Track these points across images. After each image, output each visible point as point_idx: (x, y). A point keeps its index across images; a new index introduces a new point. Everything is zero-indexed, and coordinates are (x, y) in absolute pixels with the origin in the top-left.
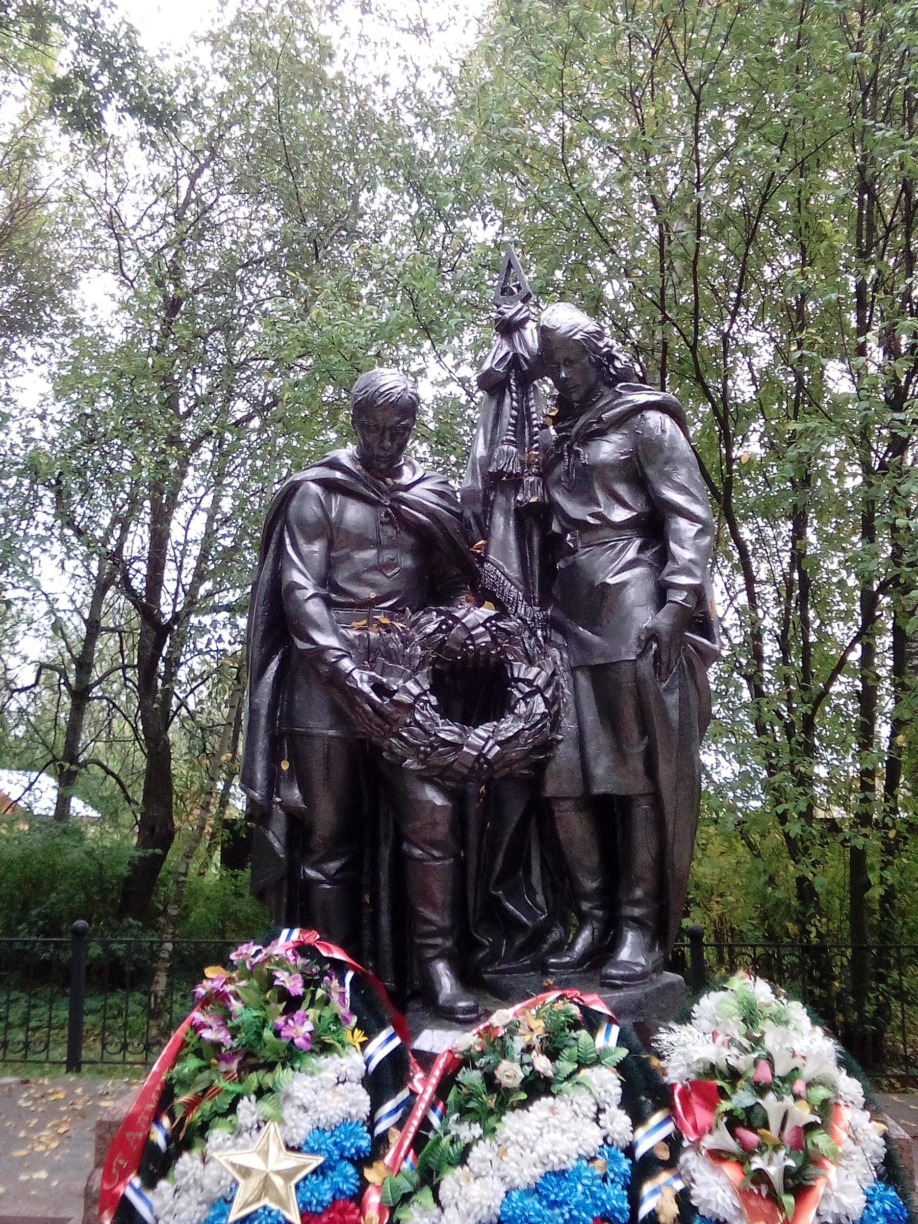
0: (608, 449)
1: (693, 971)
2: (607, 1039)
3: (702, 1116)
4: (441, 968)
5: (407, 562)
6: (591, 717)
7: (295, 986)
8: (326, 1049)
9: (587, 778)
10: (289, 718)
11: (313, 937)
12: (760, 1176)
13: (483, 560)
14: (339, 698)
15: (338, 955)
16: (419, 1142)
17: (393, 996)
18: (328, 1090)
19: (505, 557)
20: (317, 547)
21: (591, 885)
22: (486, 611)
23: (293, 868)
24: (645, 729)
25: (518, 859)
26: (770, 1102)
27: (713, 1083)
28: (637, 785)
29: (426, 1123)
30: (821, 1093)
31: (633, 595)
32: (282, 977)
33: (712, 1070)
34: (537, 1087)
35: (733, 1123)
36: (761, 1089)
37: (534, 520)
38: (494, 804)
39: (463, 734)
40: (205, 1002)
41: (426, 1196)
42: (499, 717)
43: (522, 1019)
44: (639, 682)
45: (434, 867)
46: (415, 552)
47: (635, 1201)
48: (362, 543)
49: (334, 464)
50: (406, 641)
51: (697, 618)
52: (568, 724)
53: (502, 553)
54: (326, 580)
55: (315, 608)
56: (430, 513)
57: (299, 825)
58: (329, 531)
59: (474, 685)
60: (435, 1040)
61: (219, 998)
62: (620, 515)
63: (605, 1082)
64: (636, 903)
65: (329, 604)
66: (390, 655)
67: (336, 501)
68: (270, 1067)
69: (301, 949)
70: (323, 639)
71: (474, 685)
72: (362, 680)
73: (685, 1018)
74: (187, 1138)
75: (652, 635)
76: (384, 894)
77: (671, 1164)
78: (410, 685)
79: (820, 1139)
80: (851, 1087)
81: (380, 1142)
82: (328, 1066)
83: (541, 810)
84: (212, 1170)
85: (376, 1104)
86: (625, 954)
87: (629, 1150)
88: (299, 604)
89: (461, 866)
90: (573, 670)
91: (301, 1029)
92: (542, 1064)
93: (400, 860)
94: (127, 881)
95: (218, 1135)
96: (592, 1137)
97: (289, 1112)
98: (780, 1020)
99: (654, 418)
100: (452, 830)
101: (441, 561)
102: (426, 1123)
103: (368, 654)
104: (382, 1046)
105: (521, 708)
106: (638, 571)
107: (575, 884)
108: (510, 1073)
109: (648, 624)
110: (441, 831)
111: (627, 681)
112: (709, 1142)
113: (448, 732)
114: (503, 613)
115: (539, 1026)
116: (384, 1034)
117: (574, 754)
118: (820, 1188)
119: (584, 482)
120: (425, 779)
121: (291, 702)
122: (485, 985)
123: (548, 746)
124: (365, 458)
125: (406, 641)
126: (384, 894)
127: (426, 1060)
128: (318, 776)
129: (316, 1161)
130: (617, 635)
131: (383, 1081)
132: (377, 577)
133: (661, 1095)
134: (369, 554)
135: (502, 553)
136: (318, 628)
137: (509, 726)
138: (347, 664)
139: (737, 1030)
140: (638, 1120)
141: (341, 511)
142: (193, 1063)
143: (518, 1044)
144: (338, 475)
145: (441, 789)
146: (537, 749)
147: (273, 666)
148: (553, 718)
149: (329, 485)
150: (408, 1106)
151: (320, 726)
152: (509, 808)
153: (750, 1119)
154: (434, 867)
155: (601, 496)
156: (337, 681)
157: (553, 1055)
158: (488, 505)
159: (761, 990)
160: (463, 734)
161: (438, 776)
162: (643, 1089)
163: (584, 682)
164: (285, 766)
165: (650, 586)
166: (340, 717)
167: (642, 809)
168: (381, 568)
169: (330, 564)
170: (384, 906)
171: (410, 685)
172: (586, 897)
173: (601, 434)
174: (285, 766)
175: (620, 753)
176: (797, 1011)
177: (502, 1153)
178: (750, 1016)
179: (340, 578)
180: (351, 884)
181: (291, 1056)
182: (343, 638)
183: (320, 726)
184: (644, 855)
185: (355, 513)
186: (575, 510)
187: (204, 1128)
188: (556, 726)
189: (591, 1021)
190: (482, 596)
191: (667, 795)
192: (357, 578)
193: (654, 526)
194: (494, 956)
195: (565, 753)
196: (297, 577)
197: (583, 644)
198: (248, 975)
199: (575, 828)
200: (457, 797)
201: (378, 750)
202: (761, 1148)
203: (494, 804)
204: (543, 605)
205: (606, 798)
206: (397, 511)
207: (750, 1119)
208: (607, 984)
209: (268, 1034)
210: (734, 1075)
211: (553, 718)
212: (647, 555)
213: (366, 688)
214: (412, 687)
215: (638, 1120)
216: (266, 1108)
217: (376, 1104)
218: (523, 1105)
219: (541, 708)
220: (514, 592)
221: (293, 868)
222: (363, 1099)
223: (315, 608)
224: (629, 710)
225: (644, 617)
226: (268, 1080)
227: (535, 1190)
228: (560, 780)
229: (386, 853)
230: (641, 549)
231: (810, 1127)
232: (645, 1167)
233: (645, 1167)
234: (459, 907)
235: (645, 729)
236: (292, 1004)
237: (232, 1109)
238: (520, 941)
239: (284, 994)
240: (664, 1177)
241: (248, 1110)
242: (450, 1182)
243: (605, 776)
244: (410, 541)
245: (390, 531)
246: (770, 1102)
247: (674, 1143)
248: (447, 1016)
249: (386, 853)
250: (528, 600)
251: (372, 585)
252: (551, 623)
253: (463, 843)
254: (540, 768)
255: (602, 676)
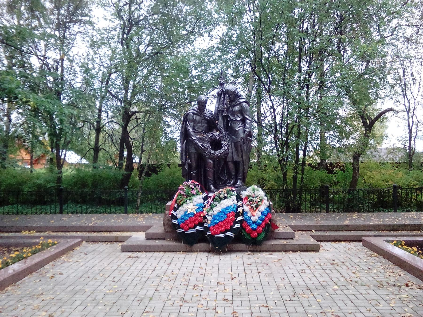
0: (237, 108)
1: (246, 185)
2: (235, 193)
3: (246, 201)
4: (211, 185)
5: (206, 125)
6: (234, 149)
7: (193, 187)
8: (197, 195)
9: (233, 159)
10: (188, 150)
11: (194, 181)
12: (252, 207)
13: (217, 124)
14: (196, 147)
15: (198, 183)
16: (210, 205)
17: (205, 188)
18: (198, 199)
19: (221, 124)
20: (192, 123)
21: (233, 174)
22: (218, 133)
23: (189, 172)
24: (242, 152)
25: (223, 170)
26: (254, 199)
27: (247, 197)
28: (240, 159)
29: (211, 203)
30: (261, 198)
31: (240, 131)
32: (191, 186)
33: (248, 196)
34: (225, 198)
35: (249, 201)
36: (253, 197)
37: (225, 118)
38: (219, 162)
39: (215, 152)
40: (180, 189)
41: (212, 210)
42: (220, 150)
43: (223, 191)
44: (241, 145)
45: (210, 172)
46: (207, 123)
47: (237, 210)
48: (199, 123)
49: (194, 110)
50: (206, 138)
51: (250, 134)
52: (230, 150)
53: (220, 124)
54: (194, 129)
55: (192, 133)
56: (209, 118)
57: (190, 166)
58: (193, 121)
59: (216, 144)
60: (211, 195)
61: (182, 189)
62: (239, 119)
63: (234, 197)
64: (240, 176)
65: (194, 132)
66: (203, 140)
67: (195, 116)
68: (191, 197)
69: (192, 182)
70: (194, 138)
71: (216, 144)
72: (200, 144)
73: (246, 190)
74: (179, 206)
75: (243, 138)
76: (202, 176)
77: (242, 206)
78: (207, 145)
79: (260, 203)
80: (266, 198)
81: (205, 206)
82: (198, 197)
83: (226, 163)
84: (184, 208)
85: (204, 202)
86: (238, 183)
87: (237, 205)
88: (190, 133)
89: (214, 171)
90: (231, 142)
91: (194, 192)
92: (226, 195)
93: (205, 171)
94: (122, 180)
95: (184, 204)
96: (232, 203)
97: (194, 202)
98: (258, 190)
99: (244, 104)
100: (213, 166)
101: (211, 124)
102: (211, 203)
103: (200, 140)
104: (204, 195)
105: (223, 148)
106: (241, 128)
107: (231, 174)
108: (222, 196)
109: (242, 136)
110: (212, 166)
111: (239, 144)
112: (246, 204)
113: (213, 152)
114: (221, 133)
115: (226, 191)
116: (205, 193)
117: (231, 155)
118: (259, 208)
119: (233, 113)
120: (209, 159)
121: (188, 147)
122: (217, 188)
123: (228, 154)
124: (199, 109)
125: (206, 138)
126: (202, 176)
127: (210, 197)
128: (193, 158)
129: (198, 207)
130: (237, 137)
131: (205, 199)
132: (201, 128)
133: (241, 199)
134: (200, 124)
135: (220, 124)
136: (193, 136)
137: (222, 151)
138: (198, 142)
139: (252, 192)
140: (238, 202)
141: (196, 118)
142: (180, 197)
143: (223, 193)
144: (195, 112)
145: (212, 160)
146: (226, 154)
147: (185, 142)
148: (228, 150)
149: (193, 113)
150: (208, 202)
151: (193, 151)
152: (222, 162)
153: (252, 200)
154: (210, 172)
155: (236, 116)
156: (196, 144)
157: (228, 194)
158: (218, 115)
159: (256, 187)
160: (215, 152)
161: (211, 158)
162: (239, 198)
163: (233, 144)
164: (188, 157)
165: (243, 130)
166: (196, 149)
167: (241, 163)
168: (202, 126)
169: (194, 126)
170: (203, 177)
171: (207, 145)
172: (233, 176)
173: (236, 106)
174: (188, 157)
175: (238, 155)
176: (260, 189)
177: (221, 204)
178: (254, 190)
179: (196, 128)
180: (197, 174)
181: (193, 195)
182: (197, 138)
183: (193, 151)
184: (241, 169)
185: (198, 118)
186: (232, 118)
187: (182, 204)
188: (228, 151)
189: (233, 191)
190: (217, 130)
191: (244, 161)
192: (198, 128)
193: (244, 121)
194: (219, 184)
195: (230, 155)
196: (189, 128)
197: (232, 138)
198: (185, 186)
199: (231, 166)
200: (214, 161)
201: (202, 154)
202: (252, 204)
203: (219, 162)
204: (227, 131)
205: (236, 161)
206: (204, 118)
207: (252, 200)
208: (235, 187)
209: (190, 193)
210: (250, 196)
211: (228, 150)
212: (242, 125)
213: (201, 146)
214: (207, 145)
215: (238, 202)
216: (191, 201)
217: (204, 202)
218: (224, 199)
219: (226, 148)
220: (222, 129)
221: (189, 172)
222: (203, 201)
223: (192, 133)
224: (239, 149)
225: (242, 135)
226: (190, 198)
227: (225, 209)
228: (229, 159)
229: (202, 170)
230: (242, 124)
231: (259, 202)
232: (239, 207)
233: (239, 207)
234: (214, 177)
235: (242, 152)
236: (193, 189)
237: (186, 201)
238: (223, 182)
239: (191, 188)
240: (241, 208)
241: (188, 201)
242: (214, 209)
243: (236, 158)
244: (206, 122)
245: (203, 121)
246: (254, 199)
247: (242, 204)
248: (213, 192)
249: (202, 170)
250: (225, 131)
251: (200, 129)
252: (228, 134)
253: (215, 168)
254: (226, 157)
255: (236, 144)
